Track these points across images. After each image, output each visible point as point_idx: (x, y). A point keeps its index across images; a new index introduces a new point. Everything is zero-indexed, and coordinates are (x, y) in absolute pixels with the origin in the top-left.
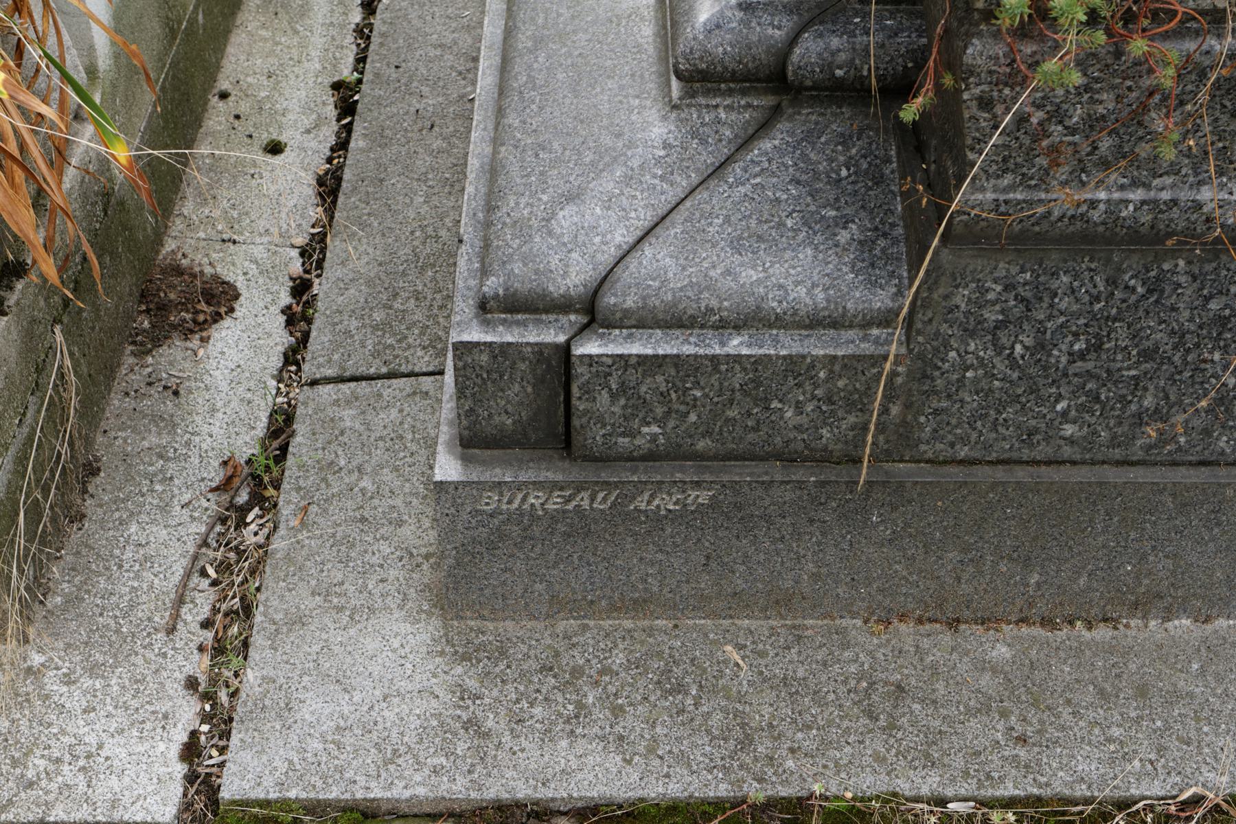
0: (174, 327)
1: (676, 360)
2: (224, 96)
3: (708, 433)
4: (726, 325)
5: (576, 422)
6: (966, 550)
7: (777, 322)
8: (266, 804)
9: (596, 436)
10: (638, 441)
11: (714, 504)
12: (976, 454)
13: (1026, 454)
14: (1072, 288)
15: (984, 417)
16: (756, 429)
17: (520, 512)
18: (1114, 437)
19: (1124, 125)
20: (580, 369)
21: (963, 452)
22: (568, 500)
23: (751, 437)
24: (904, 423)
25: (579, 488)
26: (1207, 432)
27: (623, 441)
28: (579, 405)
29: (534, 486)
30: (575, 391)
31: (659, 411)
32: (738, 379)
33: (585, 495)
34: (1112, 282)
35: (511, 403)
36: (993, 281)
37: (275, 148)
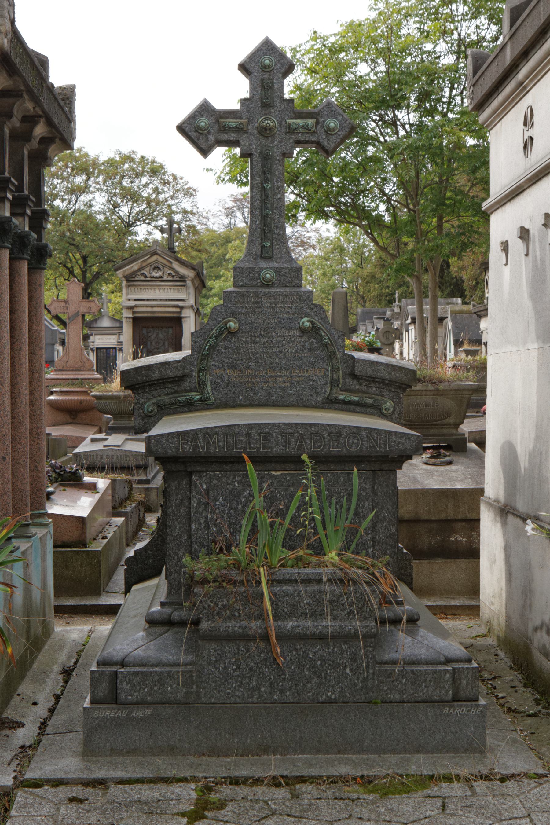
0: (7, 727)
1: (142, 673)
2: (19, 695)
3: (150, 695)
4: (153, 666)
5: (118, 692)
6: (216, 730)
7: (165, 665)
8: (35, 779)
9: (122, 696)
10: (134, 698)
11: (152, 715)
12: (216, 701)
13: (228, 701)
14: (229, 649)
15: (216, 689)
16: (162, 693)
17: (104, 717)
18: (248, 695)
19: (367, 803)
20: (119, 675)
21: (213, 700)
22: (116, 714)
23: (161, 696)
24: (197, 691)
25: (119, 710)
26: (270, 693)
27: (130, 697)
28: (119, 686)
29: (107, 712)
30: (118, 682)
31: (138, 688)
32: (156, 678)
33: (120, 712)
34: (238, 649)
35: (104, 688)
36: (212, 648)
37: (35, 704)
